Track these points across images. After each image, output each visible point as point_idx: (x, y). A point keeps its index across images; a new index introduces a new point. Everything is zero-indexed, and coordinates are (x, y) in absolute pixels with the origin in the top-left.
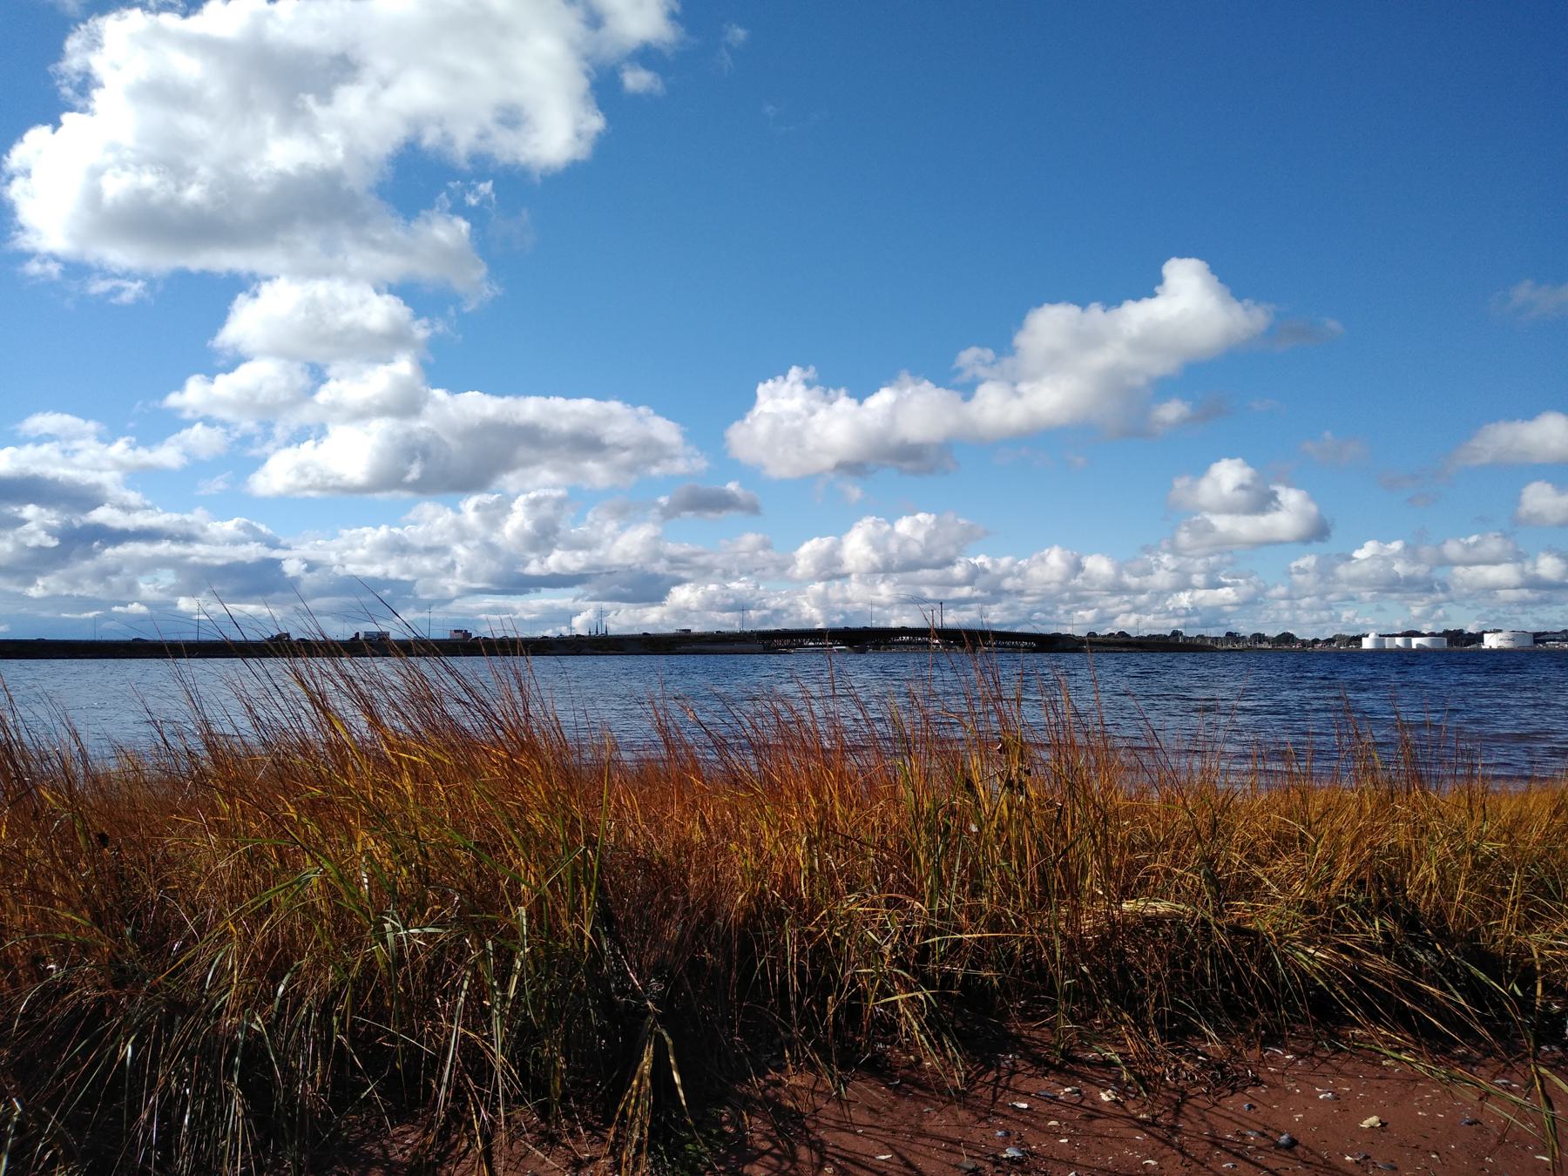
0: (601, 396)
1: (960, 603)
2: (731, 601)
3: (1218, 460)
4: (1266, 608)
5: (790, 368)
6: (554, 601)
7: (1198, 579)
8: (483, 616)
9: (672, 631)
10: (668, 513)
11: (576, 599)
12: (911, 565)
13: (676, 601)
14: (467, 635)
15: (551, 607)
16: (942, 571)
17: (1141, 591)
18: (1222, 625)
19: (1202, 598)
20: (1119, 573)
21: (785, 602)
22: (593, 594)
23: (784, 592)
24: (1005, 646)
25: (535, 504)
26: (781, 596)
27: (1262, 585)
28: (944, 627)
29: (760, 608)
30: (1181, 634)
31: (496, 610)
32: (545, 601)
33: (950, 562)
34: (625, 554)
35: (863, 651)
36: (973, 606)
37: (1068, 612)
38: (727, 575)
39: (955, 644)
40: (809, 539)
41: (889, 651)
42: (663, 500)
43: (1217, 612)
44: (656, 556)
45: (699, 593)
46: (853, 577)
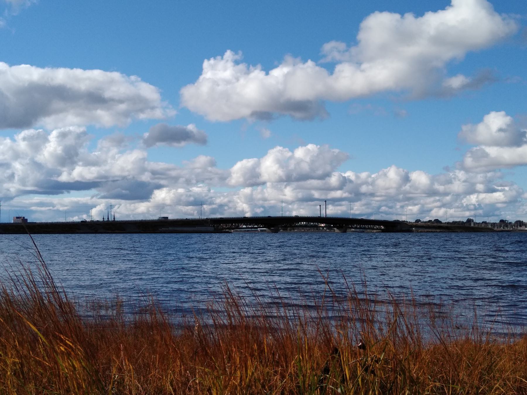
0: (106, 68)
1: (335, 201)
2: (192, 199)
3: (488, 113)
4: (523, 205)
5: (226, 51)
6: (79, 199)
7: (480, 187)
8: (33, 208)
9: (156, 218)
10: (149, 143)
11: (92, 197)
12: (304, 177)
13: (157, 199)
14: (25, 220)
15: (77, 203)
16: (324, 181)
17: (446, 194)
18: (497, 215)
19: (483, 199)
20: (432, 183)
21: (226, 200)
22: (102, 194)
23: (225, 194)
24: (365, 228)
25: (63, 135)
26: (224, 196)
27: (521, 191)
28: (328, 216)
29: (211, 204)
30: (473, 221)
31: (41, 204)
32: (75, 199)
33: (328, 175)
34: (122, 169)
35: (276, 231)
36: (344, 203)
37: (402, 207)
38: (188, 183)
39: (334, 227)
40: (241, 160)
41: (292, 231)
42: (146, 135)
43: (492, 208)
44: (143, 170)
45: (171, 194)
46: (268, 184)
